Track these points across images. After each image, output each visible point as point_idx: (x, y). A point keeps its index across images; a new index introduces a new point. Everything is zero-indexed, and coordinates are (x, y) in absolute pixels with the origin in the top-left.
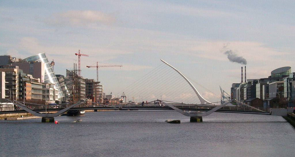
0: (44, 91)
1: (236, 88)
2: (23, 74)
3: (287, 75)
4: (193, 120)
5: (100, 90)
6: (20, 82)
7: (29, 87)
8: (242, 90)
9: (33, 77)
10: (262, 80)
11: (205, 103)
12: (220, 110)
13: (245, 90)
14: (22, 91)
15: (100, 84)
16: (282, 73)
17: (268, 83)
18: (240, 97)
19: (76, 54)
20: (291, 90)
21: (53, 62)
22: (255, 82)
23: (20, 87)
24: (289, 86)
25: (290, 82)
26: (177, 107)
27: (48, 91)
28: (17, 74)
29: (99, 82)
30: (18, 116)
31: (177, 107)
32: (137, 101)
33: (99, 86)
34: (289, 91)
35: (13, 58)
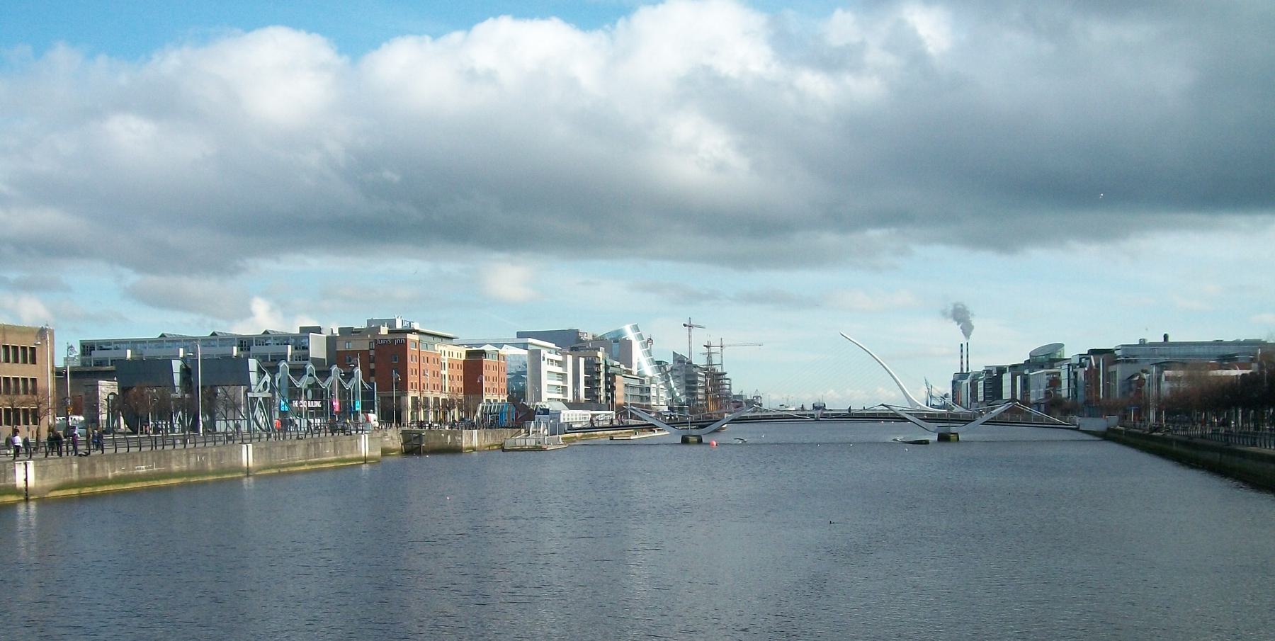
0: (641, 389)
1: (960, 381)
2: (609, 362)
3: (1057, 357)
4: (943, 438)
5: (727, 387)
6: (607, 375)
7: (620, 382)
8: (974, 385)
9: (625, 367)
10: (1014, 367)
11: (918, 408)
12: (736, 420)
13: (981, 385)
14: (611, 388)
15: (727, 376)
16: (1050, 354)
17: (1026, 372)
18: (971, 396)
19: (685, 325)
20: (1076, 383)
21: (650, 339)
22: (1001, 370)
23: (607, 383)
24: (1072, 376)
25: (1074, 370)
26: (916, 415)
27: (648, 389)
28: (602, 362)
29: (725, 373)
30: (616, 434)
31: (916, 415)
32: (842, 407)
33: (725, 379)
34: (1072, 386)
35: (584, 333)
